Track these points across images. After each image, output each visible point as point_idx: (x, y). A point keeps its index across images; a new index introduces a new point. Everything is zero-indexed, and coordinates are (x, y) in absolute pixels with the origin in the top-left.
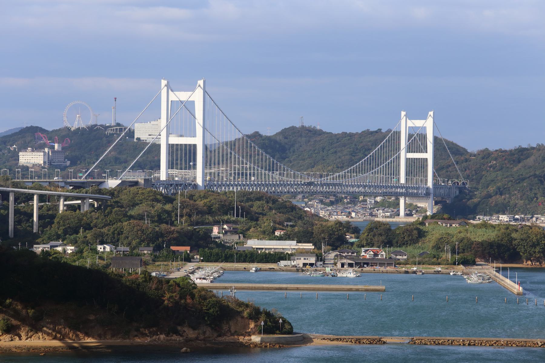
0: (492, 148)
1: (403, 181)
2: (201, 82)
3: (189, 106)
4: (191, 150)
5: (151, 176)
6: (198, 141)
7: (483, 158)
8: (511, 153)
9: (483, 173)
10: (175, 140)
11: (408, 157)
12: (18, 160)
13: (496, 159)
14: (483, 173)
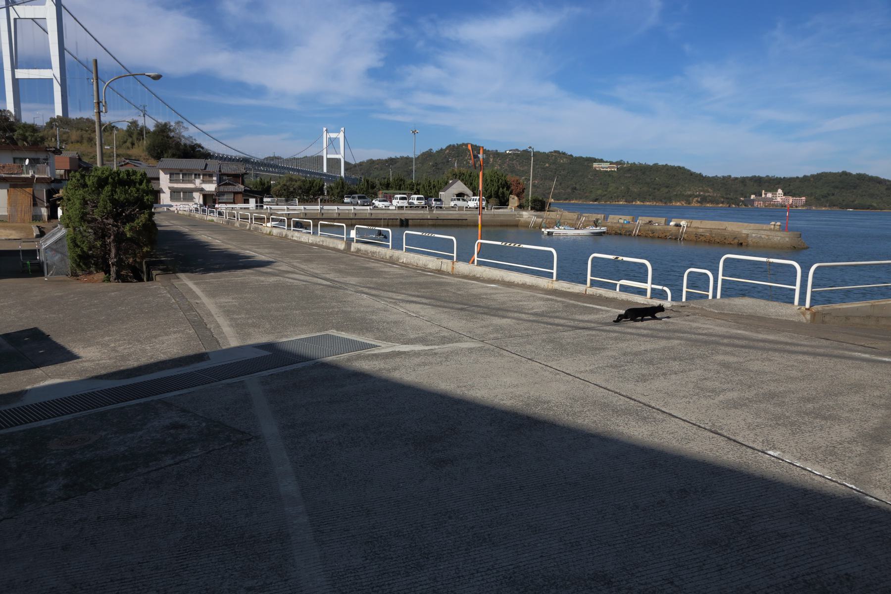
0: (375, 158)
1: (325, 170)
2: (343, 129)
3: (337, 139)
4: (339, 160)
5: (552, 198)
6: (340, 156)
7: (370, 164)
8: (386, 161)
9: (371, 172)
10: (330, 156)
11: (328, 157)
12: (461, 181)
13: (378, 164)
14: (371, 172)
